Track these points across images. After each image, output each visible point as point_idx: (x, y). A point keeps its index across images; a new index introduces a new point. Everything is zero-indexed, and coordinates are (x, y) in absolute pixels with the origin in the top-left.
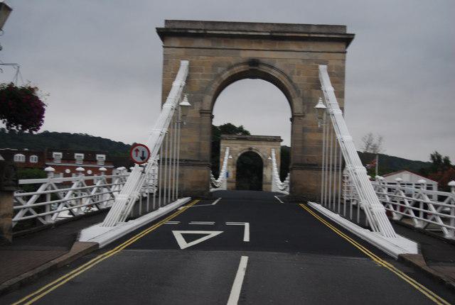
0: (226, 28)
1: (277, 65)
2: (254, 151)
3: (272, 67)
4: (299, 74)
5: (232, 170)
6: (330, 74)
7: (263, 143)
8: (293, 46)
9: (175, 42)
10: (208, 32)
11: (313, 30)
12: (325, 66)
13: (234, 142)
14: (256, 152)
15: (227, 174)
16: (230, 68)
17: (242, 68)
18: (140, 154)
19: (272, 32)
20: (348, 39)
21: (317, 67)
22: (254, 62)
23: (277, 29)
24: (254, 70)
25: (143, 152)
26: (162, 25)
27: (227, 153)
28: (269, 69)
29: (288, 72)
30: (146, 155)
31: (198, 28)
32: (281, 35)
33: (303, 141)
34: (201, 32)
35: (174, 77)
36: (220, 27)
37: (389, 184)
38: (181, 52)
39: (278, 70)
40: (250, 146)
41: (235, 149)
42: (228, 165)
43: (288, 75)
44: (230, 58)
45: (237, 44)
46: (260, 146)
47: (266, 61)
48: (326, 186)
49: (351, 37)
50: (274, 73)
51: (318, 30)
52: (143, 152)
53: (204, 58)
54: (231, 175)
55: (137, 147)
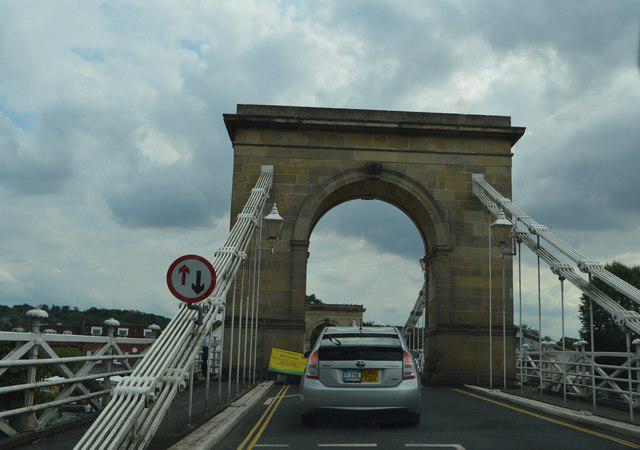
1: (410, 172)
3: (401, 175)
4: (442, 185)
8: (430, 145)
9: (253, 137)
10: (305, 122)
17: (354, 177)
18: (191, 279)
19: (400, 123)
21: (470, 176)
22: (374, 169)
24: (372, 184)
25: (199, 273)
26: (234, 111)
29: (425, 184)
30: (206, 281)
34: (292, 121)
38: (263, 152)
39: (410, 180)
45: (347, 141)
49: (519, 132)
52: (199, 273)
55: (185, 263)
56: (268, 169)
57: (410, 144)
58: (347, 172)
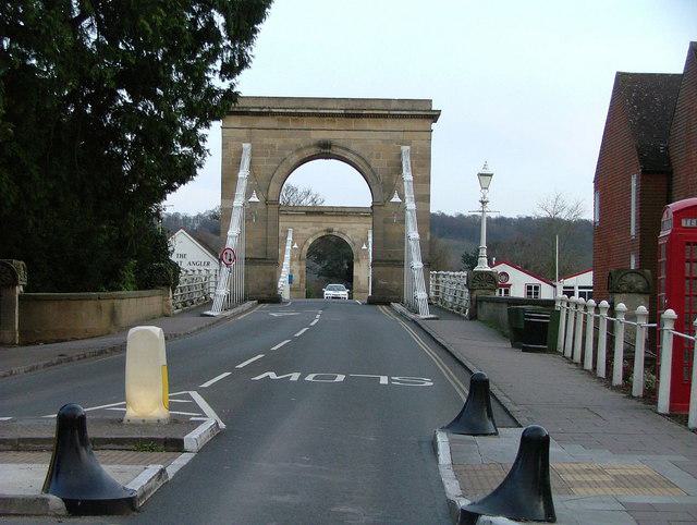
0: (294, 106)
1: (354, 147)
2: (335, 234)
3: (348, 150)
4: (378, 157)
5: (299, 268)
6: (412, 156)
7: (353, 220)
8: (368, 124)
11: (393, 106)
12: (408, 147)
13: (302, 219)
14: (341, 236)
15: (291, 277)
16: (299, 150)
17: (313, 151)
20: (434, 117)
23: (352, 105)
24: (325, 151)
27: (290, 238)
28: (345, 152)
29: (365, 154)
31: (262, 105)
32: (356, 112)
33: (385, 234)
35: (238, 164)
36: (285, 102)
37: (579, 288)
38: (243, 133)
40: (330, 226)
41: (304, 231)
42: (292, 260)
43: (366, 158)
44: (297, 140)
45: (306, 123)
46: (346, 225)
47: (341, 143)
48: (570, 334)
50: (348, 156)
51: (400, 107)
53: (267, 139)
54: (296, 277)
56: (246, 146)
57: (353, 123)
58: (309, 147)
